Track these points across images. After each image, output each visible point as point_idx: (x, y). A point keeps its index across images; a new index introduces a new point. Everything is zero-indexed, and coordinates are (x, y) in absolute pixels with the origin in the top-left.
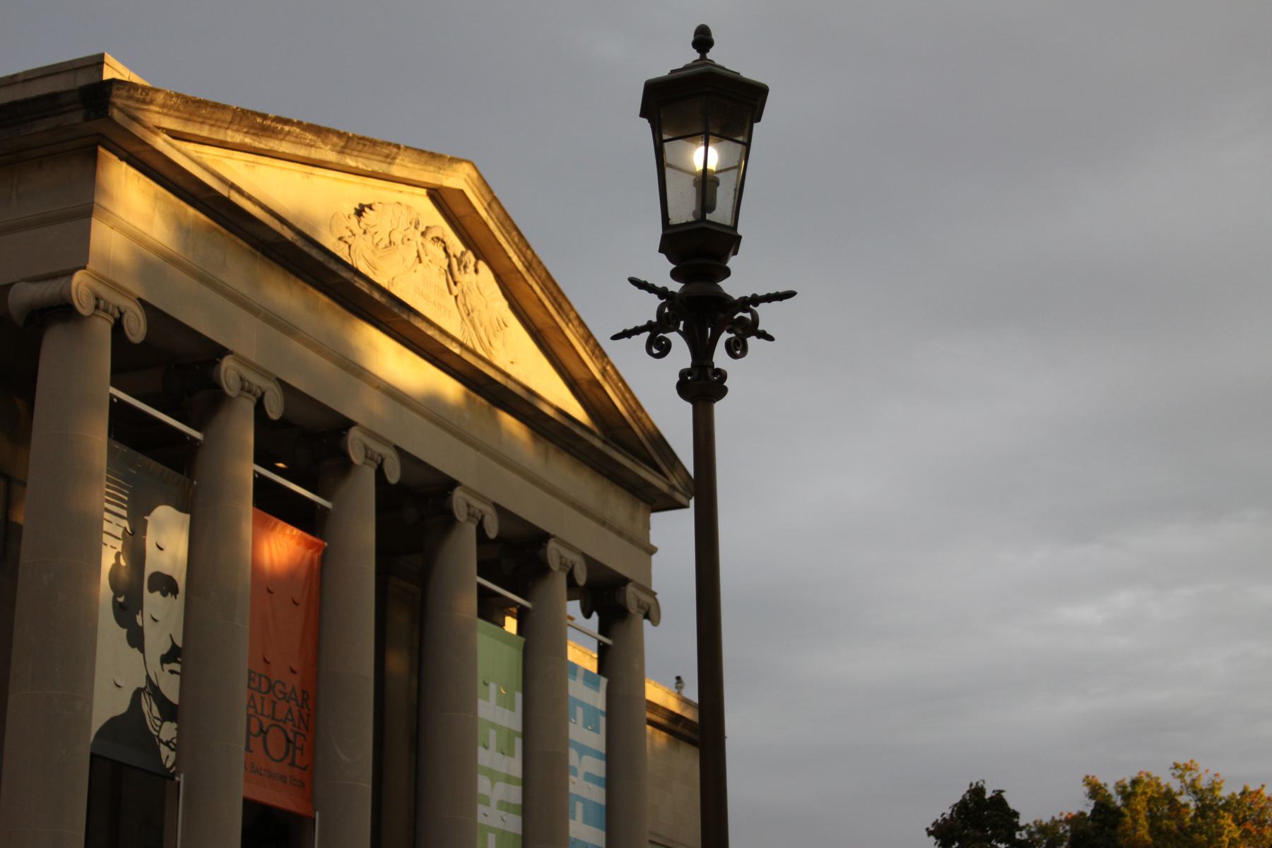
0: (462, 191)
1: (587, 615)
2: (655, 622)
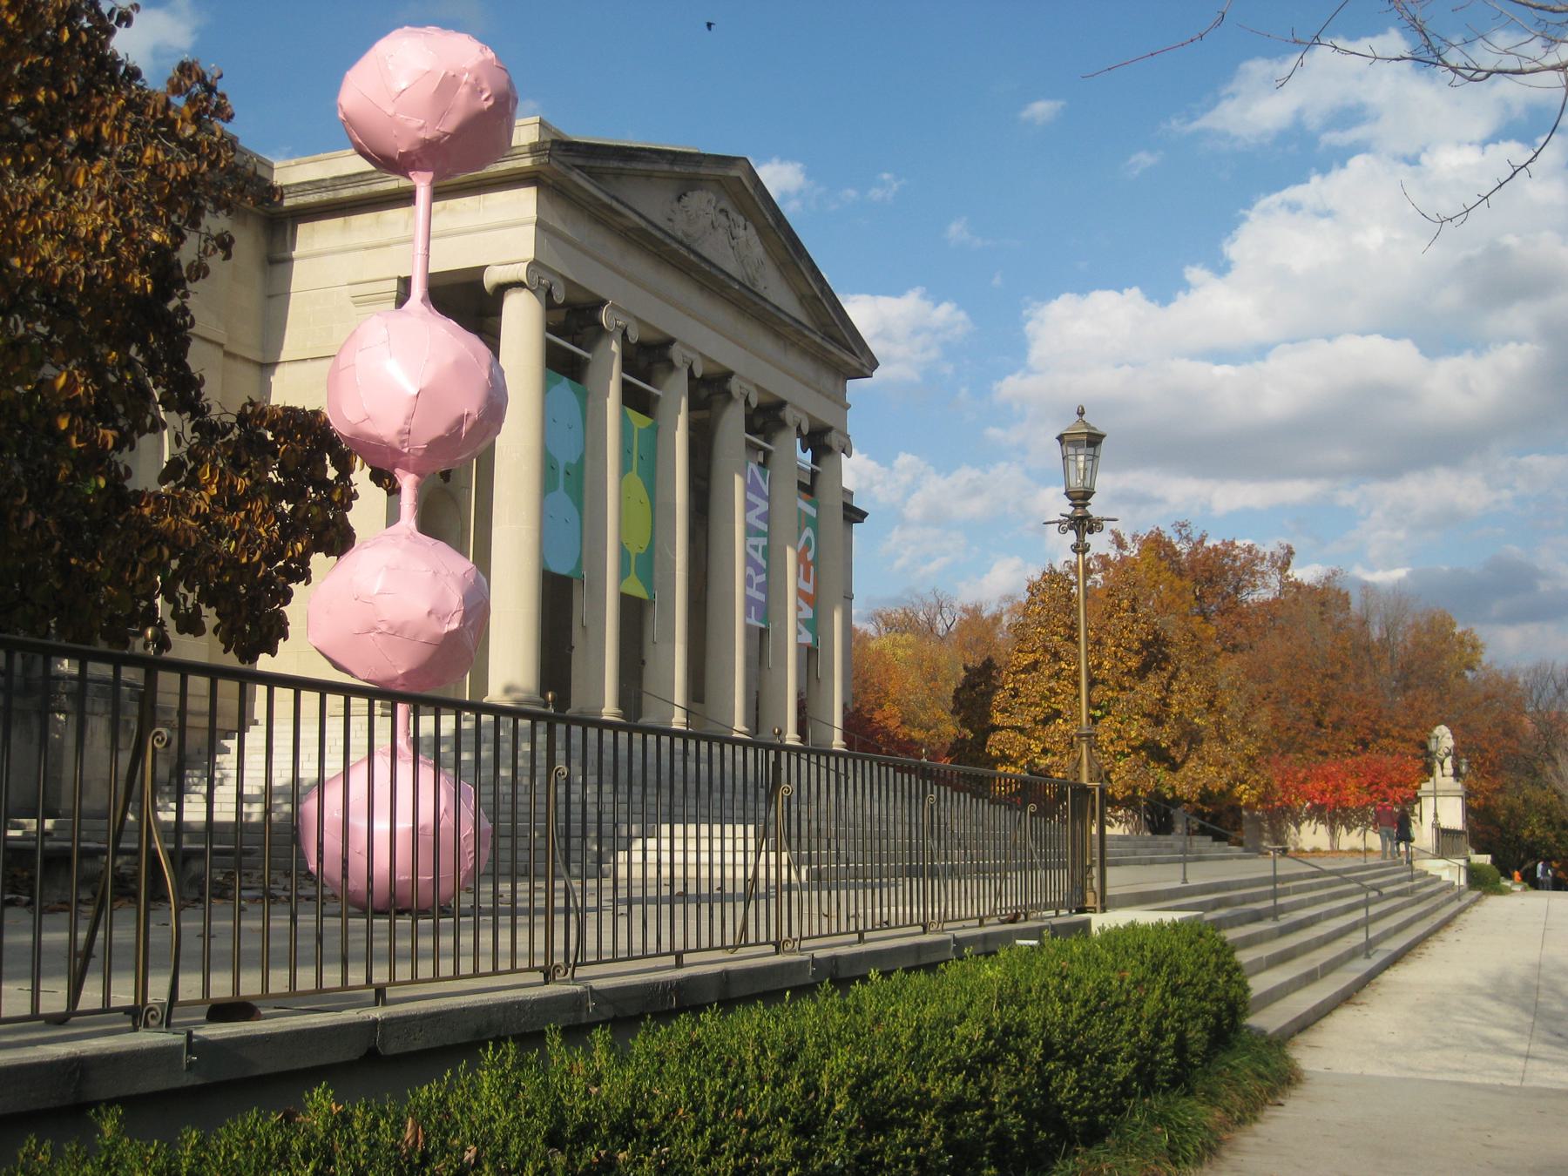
0: (739, 178)
1: (805, 451)
2: (849, 456)
